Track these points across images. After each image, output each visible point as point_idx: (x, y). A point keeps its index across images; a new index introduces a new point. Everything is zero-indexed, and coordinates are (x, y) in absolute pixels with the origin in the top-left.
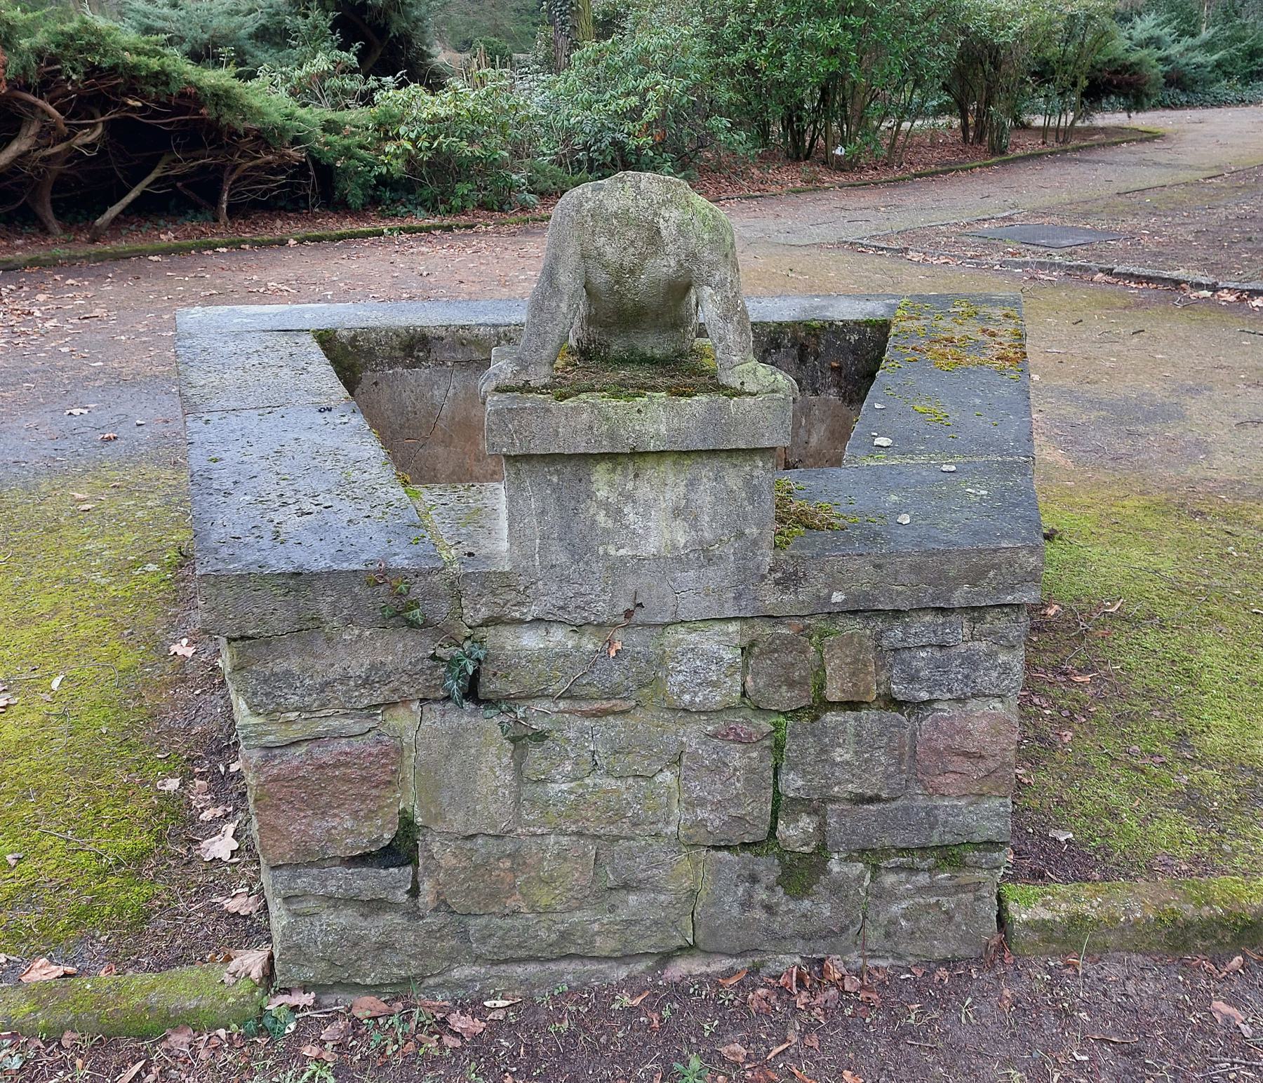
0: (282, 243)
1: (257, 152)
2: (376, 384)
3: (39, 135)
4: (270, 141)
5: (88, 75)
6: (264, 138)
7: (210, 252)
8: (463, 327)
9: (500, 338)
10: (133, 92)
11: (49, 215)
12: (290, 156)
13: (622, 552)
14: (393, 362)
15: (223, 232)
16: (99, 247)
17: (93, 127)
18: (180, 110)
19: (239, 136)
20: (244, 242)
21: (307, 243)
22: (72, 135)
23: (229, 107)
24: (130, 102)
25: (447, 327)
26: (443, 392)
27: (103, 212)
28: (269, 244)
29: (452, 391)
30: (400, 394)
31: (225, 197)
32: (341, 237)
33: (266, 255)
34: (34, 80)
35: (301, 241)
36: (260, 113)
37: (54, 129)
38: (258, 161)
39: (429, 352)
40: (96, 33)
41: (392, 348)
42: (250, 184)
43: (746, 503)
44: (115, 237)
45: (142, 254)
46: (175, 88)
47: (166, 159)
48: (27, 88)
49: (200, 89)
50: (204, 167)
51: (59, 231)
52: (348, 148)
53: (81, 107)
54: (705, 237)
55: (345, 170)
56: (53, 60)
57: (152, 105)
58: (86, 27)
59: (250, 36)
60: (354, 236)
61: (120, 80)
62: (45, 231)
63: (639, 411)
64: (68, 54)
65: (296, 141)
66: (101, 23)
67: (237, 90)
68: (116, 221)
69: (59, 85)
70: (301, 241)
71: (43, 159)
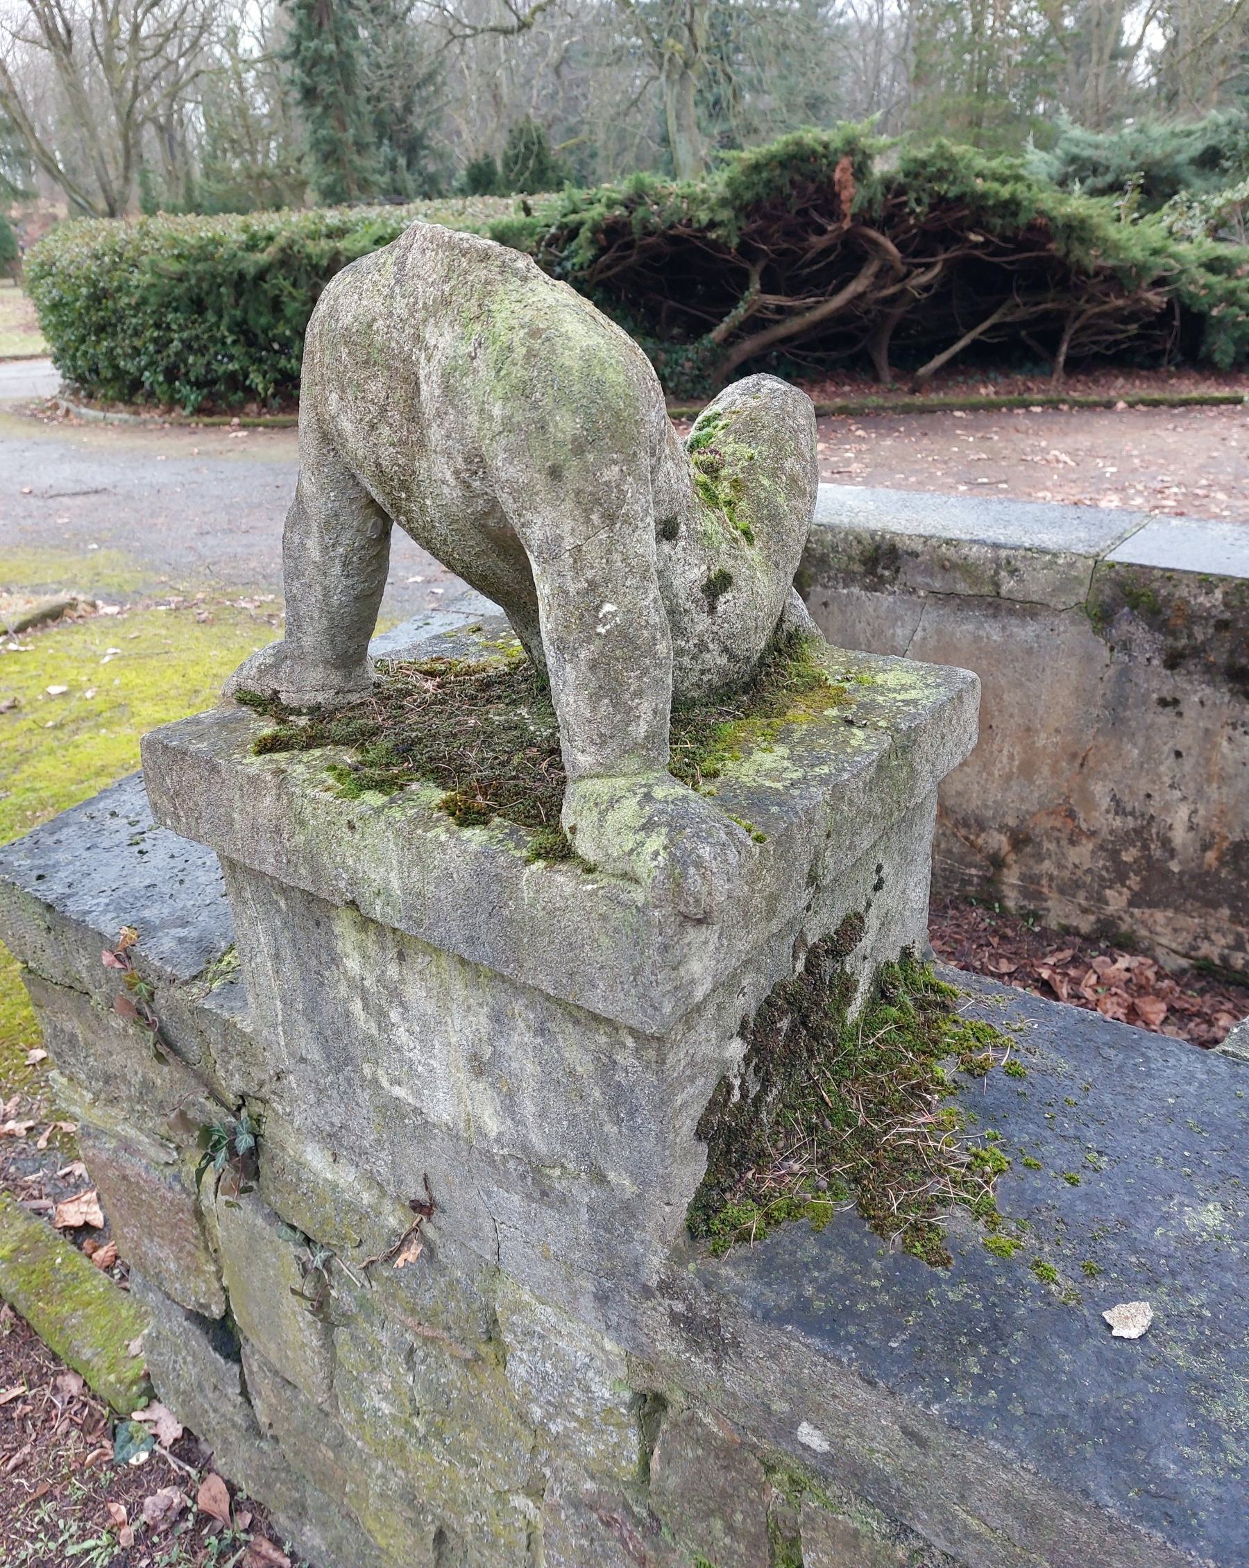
0: (1109, 405)
1: (1107, 295)
2: (826, 604)
3: (877, 276)
4: (1125, 282)
5: (933, 208)
6: (1117, 278)
7: (1021, 411)
8: (948, 542)
9: (999, 566)
10: (978, 226)
11: (882, 359)
12: (1147, 301)
13: (398, 1091)
14: (849, 578)
15: (1054, 387)
16: (919, 399)
17: (929, 266)
18: (1022, 246)
19: (1088, 276)
20: (1064, 402)
21: (1140, 407)
22: (908, 275)
23: (1082, 241)
24: (973, 237)
25: (926, 539)
26: (908, 632)
27: (931, 358)
28: (1091, 406)
29: (920, 634)
30: (853, 625)
31: (1064, 348)
32: (1185, 403)
33: (1078, 418)
34: (878, 212)
35: (1131, 405)
36: (1117, 247)
37: (892, 267)
38: (1106, 307)
39: (897, 571)
40: (952, 159)
41: (850, 558)
42: (1096, 334)
43: (603, 1114)
44: (937, 390)
45: (948, 408)
46: (1022, 219)
47: (1008, 303)
48: (871, 223)
49: (1052, 219)
50: (1047, 313)
51: (888, 379)
52: (1232, 292)
53: (919, 246)
54: (497, 411)
55: (1220, 320)
56: (902, 190)
57: (995, 240)
58: (942, 152)
59: (1193, 161)
60: (1202, 402)
61: (966, 212)
62: (877, 379)
63: (351, 827)
64: (916, 183)
65: (1160, 282)
66: (957, 149)
67: (1095, 220)
68: (937, 373)
69: (904, 220)
70: (1131, 405)
71: (877, 302)
